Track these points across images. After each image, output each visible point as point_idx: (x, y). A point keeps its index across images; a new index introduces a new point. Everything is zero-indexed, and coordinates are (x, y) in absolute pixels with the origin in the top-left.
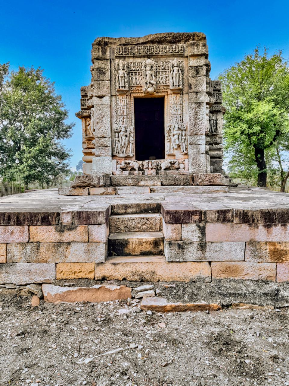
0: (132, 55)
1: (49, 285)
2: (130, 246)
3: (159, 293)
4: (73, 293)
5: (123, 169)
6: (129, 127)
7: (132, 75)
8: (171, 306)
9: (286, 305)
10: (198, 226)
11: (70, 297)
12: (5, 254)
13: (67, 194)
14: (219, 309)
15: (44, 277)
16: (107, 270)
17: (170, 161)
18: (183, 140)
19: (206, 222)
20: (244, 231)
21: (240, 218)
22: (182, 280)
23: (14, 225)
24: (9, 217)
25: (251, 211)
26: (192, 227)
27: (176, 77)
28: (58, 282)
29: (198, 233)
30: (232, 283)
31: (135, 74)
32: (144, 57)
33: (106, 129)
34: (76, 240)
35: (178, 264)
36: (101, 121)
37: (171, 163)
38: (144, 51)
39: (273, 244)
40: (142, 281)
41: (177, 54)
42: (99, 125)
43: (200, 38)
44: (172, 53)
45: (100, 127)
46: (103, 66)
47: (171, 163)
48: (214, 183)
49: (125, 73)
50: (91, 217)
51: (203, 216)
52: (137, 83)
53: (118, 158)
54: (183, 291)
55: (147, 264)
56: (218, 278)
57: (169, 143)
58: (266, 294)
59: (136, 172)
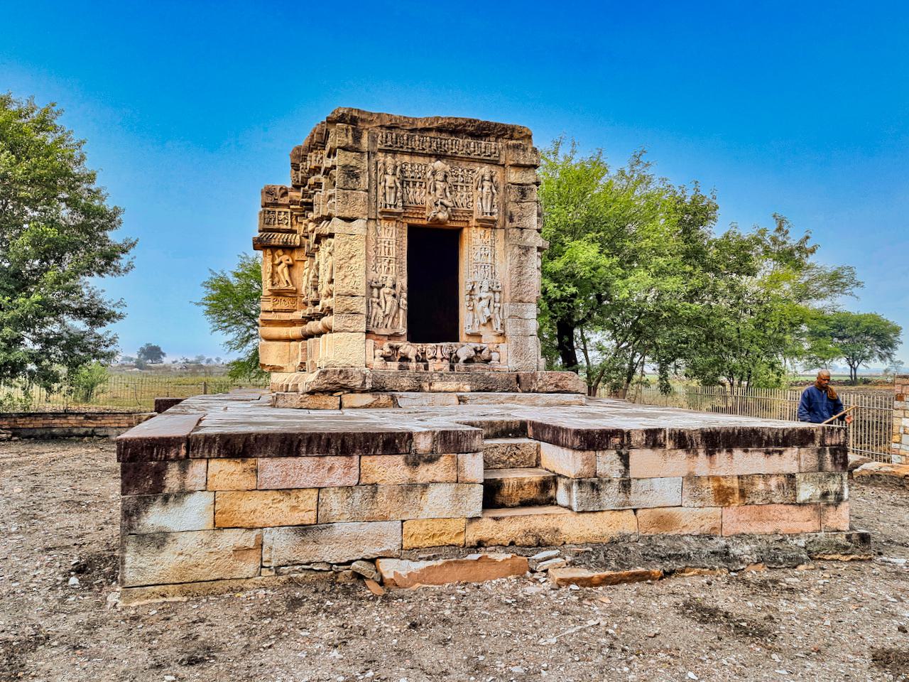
0: (410, 150)
1: (391, 560)
2: (505, 491)
3: (570, 562)
4: (437, 570)
5: (387, 358)
6: (398, 280)
7: (408, 185)
8: (599, 577)
9: (742, 568)
10: (620, 454)
11: (434, 576)
12: (315, 507)
13: (294, 406)
14: (661, 578)
15: (381, 546)
16: (487, 528)
17: (474, 345)
18: (497, 309)
19: (631, 447)
20: (679, 461)
21: (675, 440)
22: (599, 540)
23: (337, 455)
24: (329, 440)
25: (689, 431)
26: (611, 455)
27: (487, 198)
28: (406, 553)
29: (618, 466)
30: (667, 540)
31: (414, 185)
32: (430, 156)
33: (357, 280)
34: (437, 479)
35: (592, 515)
36: (347, 265)
37: (475, 349)
38: (430, 147)
39: (716, 479)
40: (539, 545)
41: (488, 158)
42: (343, 272)
43: (522, 135)
44: (479, 155)
45: (345, 276)
46: (354, 163)
47: (475, 349)
48: (564, 389)
49: (397, 180)
50: (463, 440)
51: (625, 438)
52: (418, 202)
53: (375, 337)
54: (605, 556)
55: (546, 517)
56: (647, 534)
57: (471, 313)
58: (714, 553)
59: (413, 365)
